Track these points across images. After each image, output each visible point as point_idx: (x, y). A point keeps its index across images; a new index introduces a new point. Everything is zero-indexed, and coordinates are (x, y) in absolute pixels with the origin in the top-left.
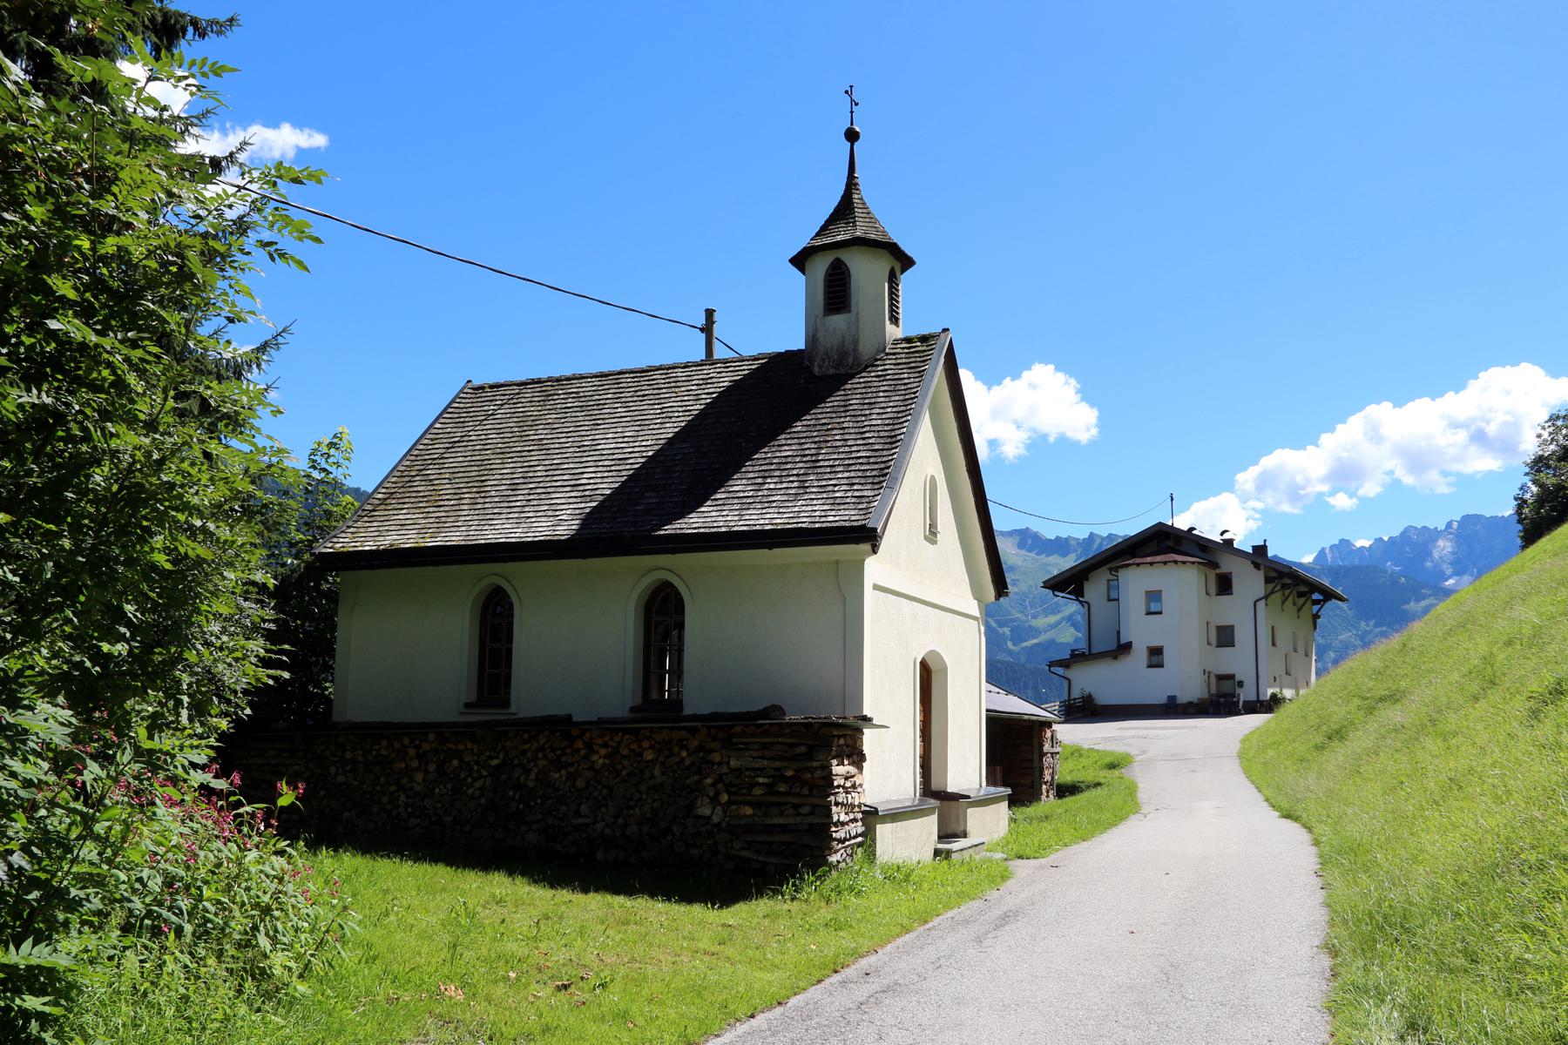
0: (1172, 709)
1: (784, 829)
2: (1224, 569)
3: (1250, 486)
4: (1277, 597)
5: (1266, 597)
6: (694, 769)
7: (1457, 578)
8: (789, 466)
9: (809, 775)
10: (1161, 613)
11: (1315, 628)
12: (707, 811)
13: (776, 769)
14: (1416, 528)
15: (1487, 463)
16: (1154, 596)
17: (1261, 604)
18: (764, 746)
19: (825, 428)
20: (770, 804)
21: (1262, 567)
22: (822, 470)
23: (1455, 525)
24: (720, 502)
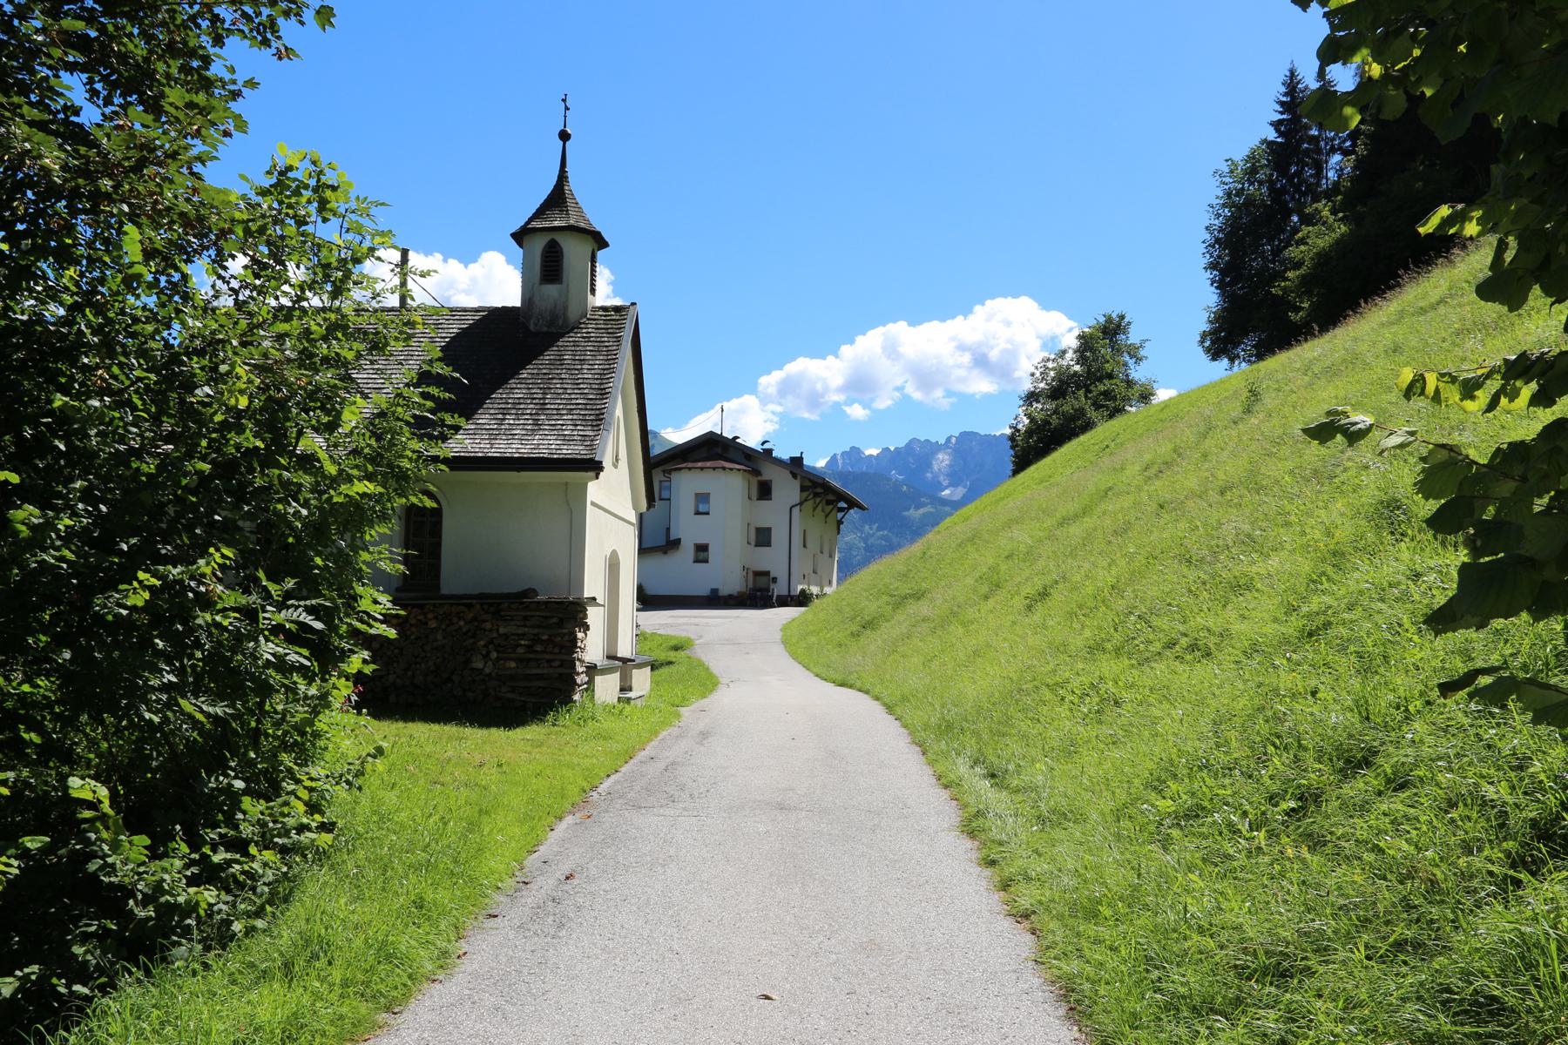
0: (715, 600)
1: (540, 677)
2: (765, 477)
3: (772, 390)
4: (809, 504)
5: (801, 504)
6: (470, 634)
7: (952, 489)
8: (522, 406)
9: (559, 639)
10: (708, 513)
11: (839, 533)
12: (479, 665)
13: (535, 635)
14: (919, 440)
15: (983, 386)
16: (702, 498)
17: (796, 511)
18: (526, 618)
19: (546, 377)
20: (530, 660)
21: (799, 477)
22: (550, 412)
23: (953, 440)
24: (471, 432)
